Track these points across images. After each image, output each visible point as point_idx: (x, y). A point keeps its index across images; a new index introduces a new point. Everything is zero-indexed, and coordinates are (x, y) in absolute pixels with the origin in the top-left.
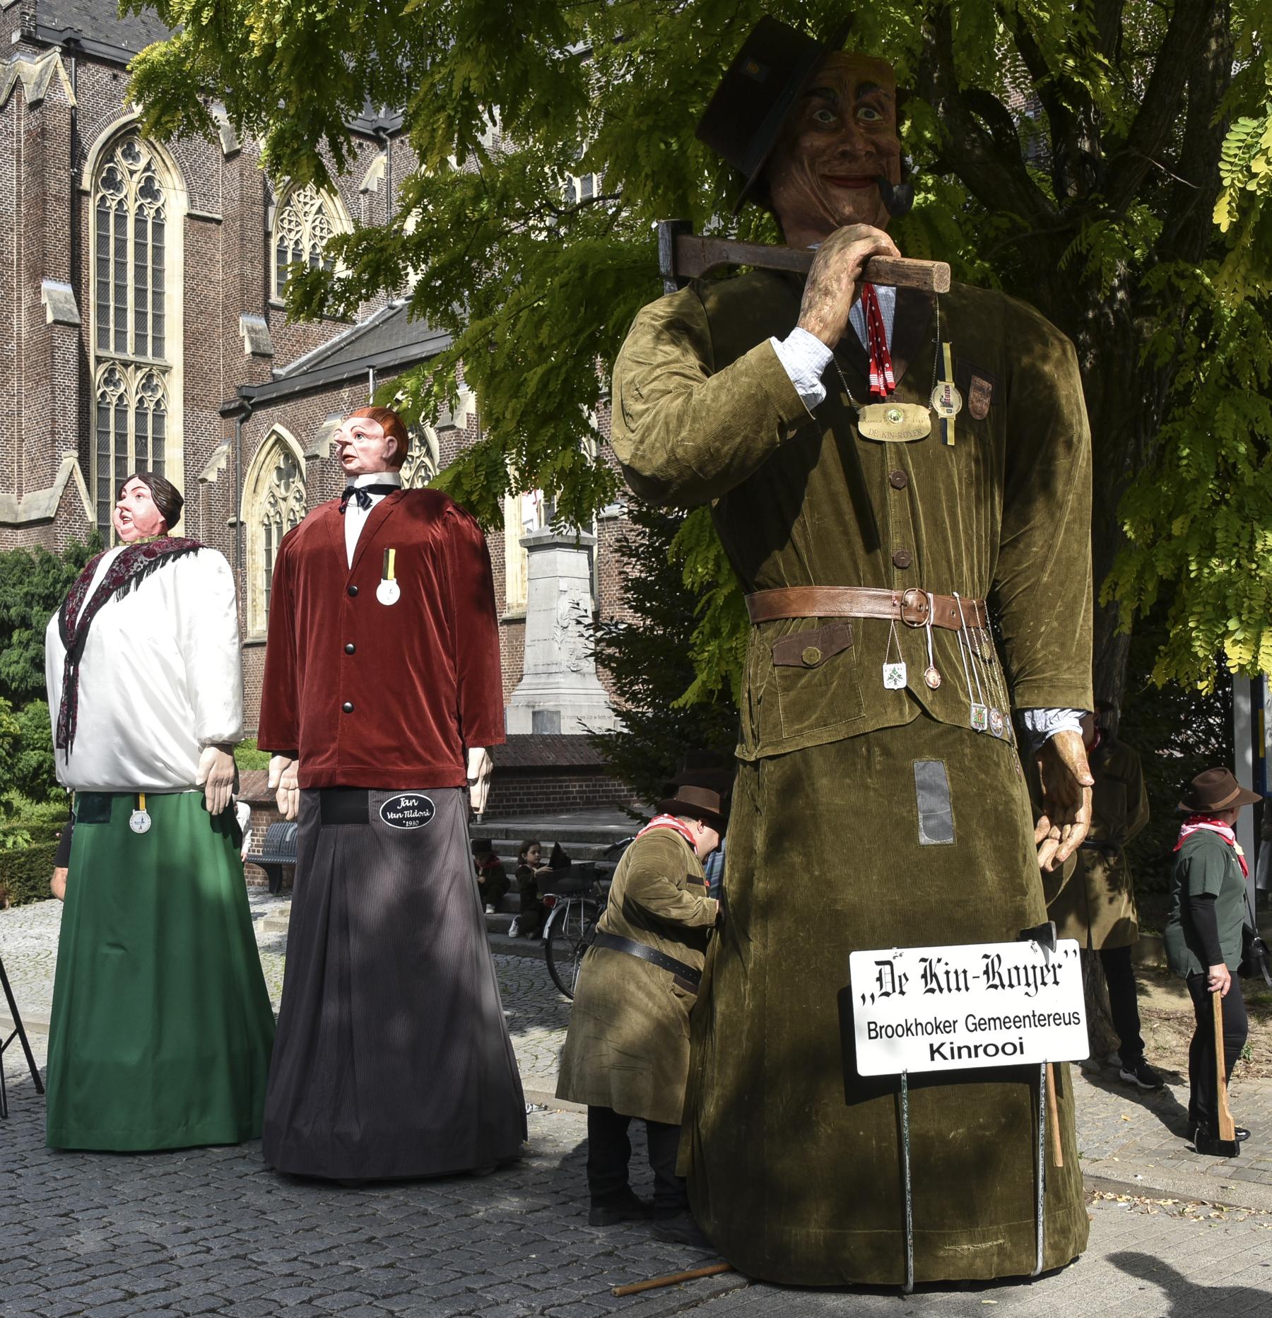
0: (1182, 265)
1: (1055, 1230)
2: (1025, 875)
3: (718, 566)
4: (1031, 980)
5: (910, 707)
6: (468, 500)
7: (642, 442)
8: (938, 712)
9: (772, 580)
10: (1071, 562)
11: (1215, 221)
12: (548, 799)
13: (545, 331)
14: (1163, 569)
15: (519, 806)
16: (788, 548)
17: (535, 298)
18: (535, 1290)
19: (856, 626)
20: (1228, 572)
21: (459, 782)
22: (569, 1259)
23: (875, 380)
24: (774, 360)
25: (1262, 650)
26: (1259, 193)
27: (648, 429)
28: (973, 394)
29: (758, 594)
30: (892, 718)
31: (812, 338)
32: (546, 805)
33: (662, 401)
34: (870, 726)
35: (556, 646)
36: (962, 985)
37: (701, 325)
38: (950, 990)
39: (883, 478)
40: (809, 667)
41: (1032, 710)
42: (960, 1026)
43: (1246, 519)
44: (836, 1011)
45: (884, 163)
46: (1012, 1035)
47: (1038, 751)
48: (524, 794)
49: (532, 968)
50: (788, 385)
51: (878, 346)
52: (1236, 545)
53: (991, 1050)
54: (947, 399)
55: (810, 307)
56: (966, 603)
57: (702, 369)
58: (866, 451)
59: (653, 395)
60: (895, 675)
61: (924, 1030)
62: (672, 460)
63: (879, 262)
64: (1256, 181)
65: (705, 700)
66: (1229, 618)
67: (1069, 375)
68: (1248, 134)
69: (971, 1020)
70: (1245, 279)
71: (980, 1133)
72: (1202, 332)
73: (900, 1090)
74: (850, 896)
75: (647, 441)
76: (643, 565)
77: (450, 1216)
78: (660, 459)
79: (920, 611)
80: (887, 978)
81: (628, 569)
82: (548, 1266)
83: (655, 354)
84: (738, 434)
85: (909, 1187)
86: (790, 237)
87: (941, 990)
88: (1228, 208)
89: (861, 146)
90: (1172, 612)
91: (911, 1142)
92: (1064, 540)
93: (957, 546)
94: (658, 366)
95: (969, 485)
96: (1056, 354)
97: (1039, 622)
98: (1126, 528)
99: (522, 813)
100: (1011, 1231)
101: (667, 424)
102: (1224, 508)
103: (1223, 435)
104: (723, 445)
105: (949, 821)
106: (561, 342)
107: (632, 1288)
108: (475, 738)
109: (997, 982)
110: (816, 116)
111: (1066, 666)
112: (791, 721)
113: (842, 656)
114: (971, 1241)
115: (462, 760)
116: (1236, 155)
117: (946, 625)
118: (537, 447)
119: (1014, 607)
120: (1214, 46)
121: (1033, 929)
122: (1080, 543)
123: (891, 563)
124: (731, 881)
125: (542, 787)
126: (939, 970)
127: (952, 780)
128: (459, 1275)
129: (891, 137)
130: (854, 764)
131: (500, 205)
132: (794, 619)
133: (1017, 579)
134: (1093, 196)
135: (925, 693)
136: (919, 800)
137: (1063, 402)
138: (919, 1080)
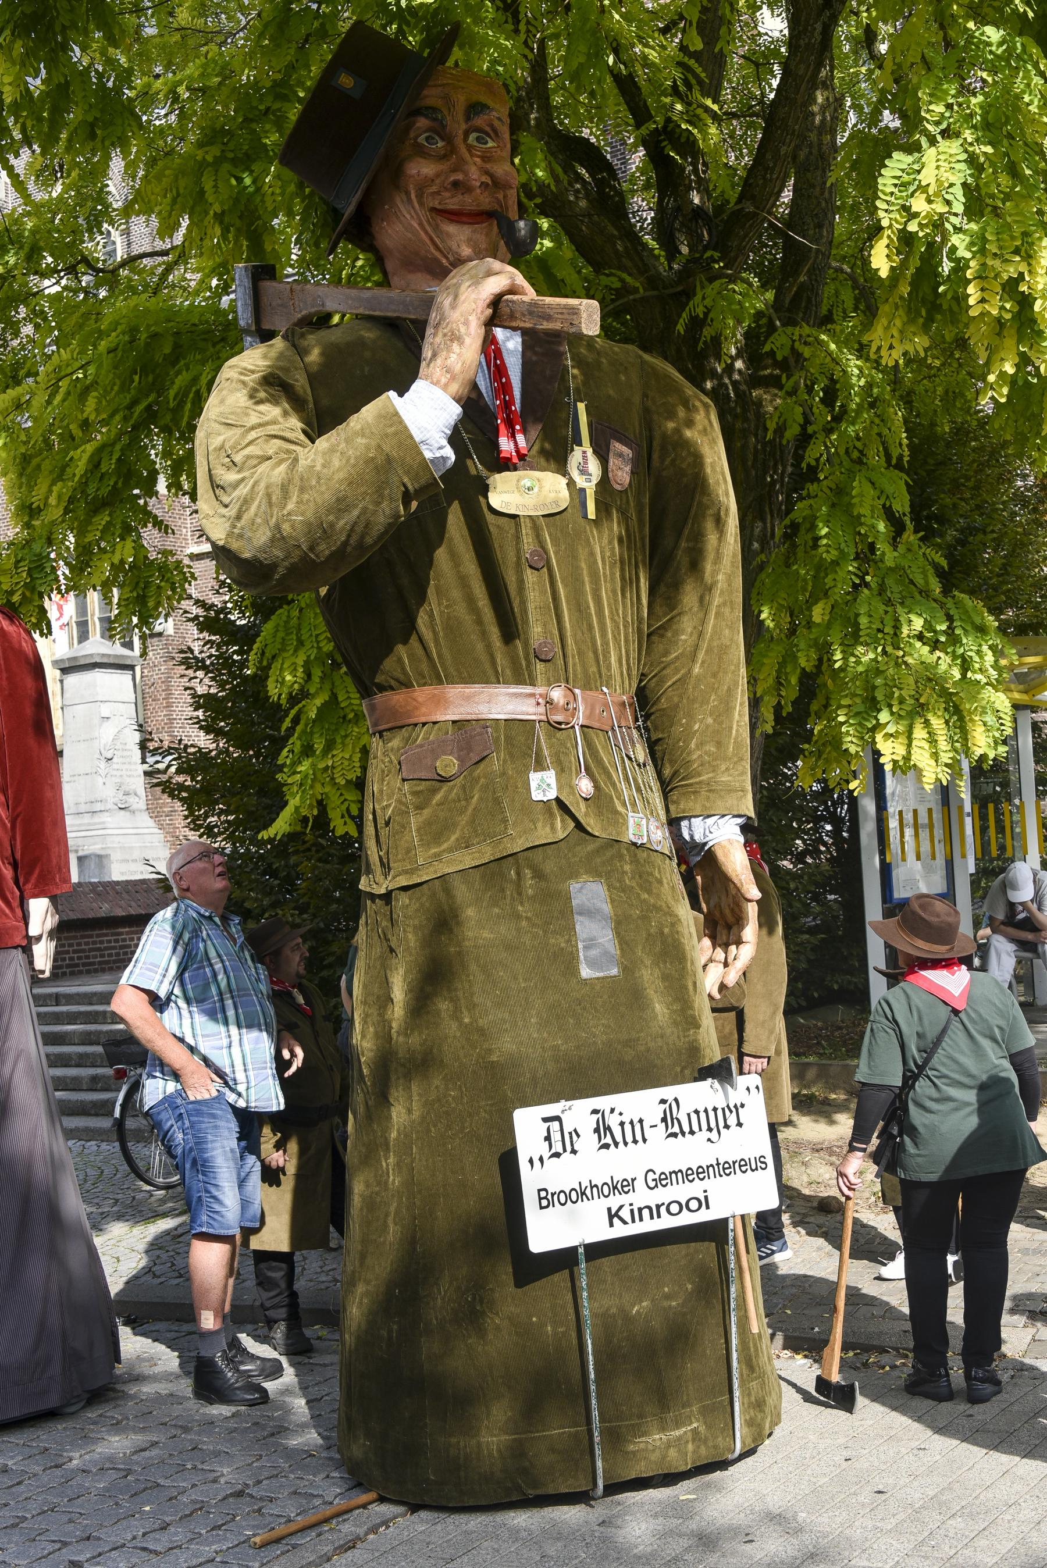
0: (807, 330)
1: (750, 1403)
2: (696, 1006)
3: (309, 676)
4: (713, 1124)
5: (562, 821)
6: (8, 601)
7: (238, 517)
8: (592, 824)
9: (397, 680)
10: (724, 650)
11: (874, 266)
12: (102, 956)
13: (91, 403)
14: (805, 661)
15: (68, 966)
16: (413, 640)
17: (78, 364)
18: (156, 1553)
19: (497, 729)
20: (875, 660)
21: (19, 940)
22: (191, 1508)
23: (505, 445)
24: (395, 417)
25: (914, 743)
26: (921, 234)
27: (246, 502)
28: (613, 462)
29: (379, 698)
30: (543, 835)
31: (438, 392)
32: (100, 963)
33: (261, 469)
34: (518, 845)
35: (100, 780)
36: (639, 1137)
37: (300, 382)
38: (626, 1144)
39: (519, 558)
40: (444, 780)
41: (689, 818)
42: (640, 1184)
43: (889, 602)
44: (498, 1180)
45: (501, 196)
46: (696, 1189)
47: (698, 865)
48: (74, 952)
49: (98, 1153)
50: (414, 448)
51: (507, 405)
52: (879, 630)
53: (674, 1208)
54: (585, 466)
55: (434, 355)
56: (616, 700)
57: (304, 432)
58: (498, 527)
59: (251, 465)
60: (543, 785)
61: (601, 1193)
62: (278, 538)
63: (513, 302)
64: (917, 221)
65: (299, 828)
66: (879, 710)
67: (714, 441)
68: (903, 170)
69: (651, 1176)
70: (901, 332)
71: (666, 1304)
72: (829, 399)
73: (577, 1264)
74: (506, 1045)
75: (245, 517)
76: (213, 679)
77: (38, 1469)
78: (262, 537)
79: (567, 710)
80: (556, 1137)
81: (195, 683)
82: (168, 1519)
83: (247, 415)
84: (355, 506)
85: (592, 1376)
86: (395, 280)
87: (616, 1144)
88: (886, 251)
89: (474, 175)
90: (815, 706)
91: (593, 1325)
92: (714, 626)
93: (604, 635)
94: (253, 428)
95: (612, 566)
96: (700, 417)
97: (691, 716)
98: (763, 616)
99: (72, 974)
100: (706, 1412)
101: (269, 496)
102: (866, 591)
103: (862, 511)
104: (338, 519)
105: (612, 950)
106: (112, 416)
107: (274, 1535)
108: (36, 886)
109: (676, 1129)
110: (421, 139)
111: (723, 767)
112: (426, 845)
113: (482, 765)
114: (663, 1429)
115: (20, 914)
116: (892, 194)
117: (596, 725)
118: (90, 538)
119: (663, 703)
120: (820, 100)
121: (711, 1066)
122: (730, 628)
123: (532, 656)
124: (363, 1036)
125: (94, 943)
126: (613, 1121)
127: (612, 901)
128: (57, 1546)
129: (507, 167)
130: (503, 890)
131: (29, 258)
132: (424, 724)
133: (665, 672)
134: (708, 254)
135: (578, 803)
136: (578, 927)
137: (708, 470)
138: (596, 1251)
